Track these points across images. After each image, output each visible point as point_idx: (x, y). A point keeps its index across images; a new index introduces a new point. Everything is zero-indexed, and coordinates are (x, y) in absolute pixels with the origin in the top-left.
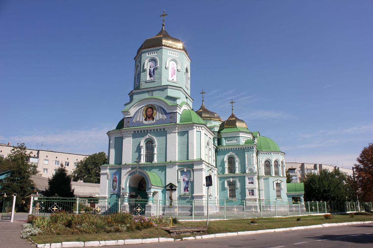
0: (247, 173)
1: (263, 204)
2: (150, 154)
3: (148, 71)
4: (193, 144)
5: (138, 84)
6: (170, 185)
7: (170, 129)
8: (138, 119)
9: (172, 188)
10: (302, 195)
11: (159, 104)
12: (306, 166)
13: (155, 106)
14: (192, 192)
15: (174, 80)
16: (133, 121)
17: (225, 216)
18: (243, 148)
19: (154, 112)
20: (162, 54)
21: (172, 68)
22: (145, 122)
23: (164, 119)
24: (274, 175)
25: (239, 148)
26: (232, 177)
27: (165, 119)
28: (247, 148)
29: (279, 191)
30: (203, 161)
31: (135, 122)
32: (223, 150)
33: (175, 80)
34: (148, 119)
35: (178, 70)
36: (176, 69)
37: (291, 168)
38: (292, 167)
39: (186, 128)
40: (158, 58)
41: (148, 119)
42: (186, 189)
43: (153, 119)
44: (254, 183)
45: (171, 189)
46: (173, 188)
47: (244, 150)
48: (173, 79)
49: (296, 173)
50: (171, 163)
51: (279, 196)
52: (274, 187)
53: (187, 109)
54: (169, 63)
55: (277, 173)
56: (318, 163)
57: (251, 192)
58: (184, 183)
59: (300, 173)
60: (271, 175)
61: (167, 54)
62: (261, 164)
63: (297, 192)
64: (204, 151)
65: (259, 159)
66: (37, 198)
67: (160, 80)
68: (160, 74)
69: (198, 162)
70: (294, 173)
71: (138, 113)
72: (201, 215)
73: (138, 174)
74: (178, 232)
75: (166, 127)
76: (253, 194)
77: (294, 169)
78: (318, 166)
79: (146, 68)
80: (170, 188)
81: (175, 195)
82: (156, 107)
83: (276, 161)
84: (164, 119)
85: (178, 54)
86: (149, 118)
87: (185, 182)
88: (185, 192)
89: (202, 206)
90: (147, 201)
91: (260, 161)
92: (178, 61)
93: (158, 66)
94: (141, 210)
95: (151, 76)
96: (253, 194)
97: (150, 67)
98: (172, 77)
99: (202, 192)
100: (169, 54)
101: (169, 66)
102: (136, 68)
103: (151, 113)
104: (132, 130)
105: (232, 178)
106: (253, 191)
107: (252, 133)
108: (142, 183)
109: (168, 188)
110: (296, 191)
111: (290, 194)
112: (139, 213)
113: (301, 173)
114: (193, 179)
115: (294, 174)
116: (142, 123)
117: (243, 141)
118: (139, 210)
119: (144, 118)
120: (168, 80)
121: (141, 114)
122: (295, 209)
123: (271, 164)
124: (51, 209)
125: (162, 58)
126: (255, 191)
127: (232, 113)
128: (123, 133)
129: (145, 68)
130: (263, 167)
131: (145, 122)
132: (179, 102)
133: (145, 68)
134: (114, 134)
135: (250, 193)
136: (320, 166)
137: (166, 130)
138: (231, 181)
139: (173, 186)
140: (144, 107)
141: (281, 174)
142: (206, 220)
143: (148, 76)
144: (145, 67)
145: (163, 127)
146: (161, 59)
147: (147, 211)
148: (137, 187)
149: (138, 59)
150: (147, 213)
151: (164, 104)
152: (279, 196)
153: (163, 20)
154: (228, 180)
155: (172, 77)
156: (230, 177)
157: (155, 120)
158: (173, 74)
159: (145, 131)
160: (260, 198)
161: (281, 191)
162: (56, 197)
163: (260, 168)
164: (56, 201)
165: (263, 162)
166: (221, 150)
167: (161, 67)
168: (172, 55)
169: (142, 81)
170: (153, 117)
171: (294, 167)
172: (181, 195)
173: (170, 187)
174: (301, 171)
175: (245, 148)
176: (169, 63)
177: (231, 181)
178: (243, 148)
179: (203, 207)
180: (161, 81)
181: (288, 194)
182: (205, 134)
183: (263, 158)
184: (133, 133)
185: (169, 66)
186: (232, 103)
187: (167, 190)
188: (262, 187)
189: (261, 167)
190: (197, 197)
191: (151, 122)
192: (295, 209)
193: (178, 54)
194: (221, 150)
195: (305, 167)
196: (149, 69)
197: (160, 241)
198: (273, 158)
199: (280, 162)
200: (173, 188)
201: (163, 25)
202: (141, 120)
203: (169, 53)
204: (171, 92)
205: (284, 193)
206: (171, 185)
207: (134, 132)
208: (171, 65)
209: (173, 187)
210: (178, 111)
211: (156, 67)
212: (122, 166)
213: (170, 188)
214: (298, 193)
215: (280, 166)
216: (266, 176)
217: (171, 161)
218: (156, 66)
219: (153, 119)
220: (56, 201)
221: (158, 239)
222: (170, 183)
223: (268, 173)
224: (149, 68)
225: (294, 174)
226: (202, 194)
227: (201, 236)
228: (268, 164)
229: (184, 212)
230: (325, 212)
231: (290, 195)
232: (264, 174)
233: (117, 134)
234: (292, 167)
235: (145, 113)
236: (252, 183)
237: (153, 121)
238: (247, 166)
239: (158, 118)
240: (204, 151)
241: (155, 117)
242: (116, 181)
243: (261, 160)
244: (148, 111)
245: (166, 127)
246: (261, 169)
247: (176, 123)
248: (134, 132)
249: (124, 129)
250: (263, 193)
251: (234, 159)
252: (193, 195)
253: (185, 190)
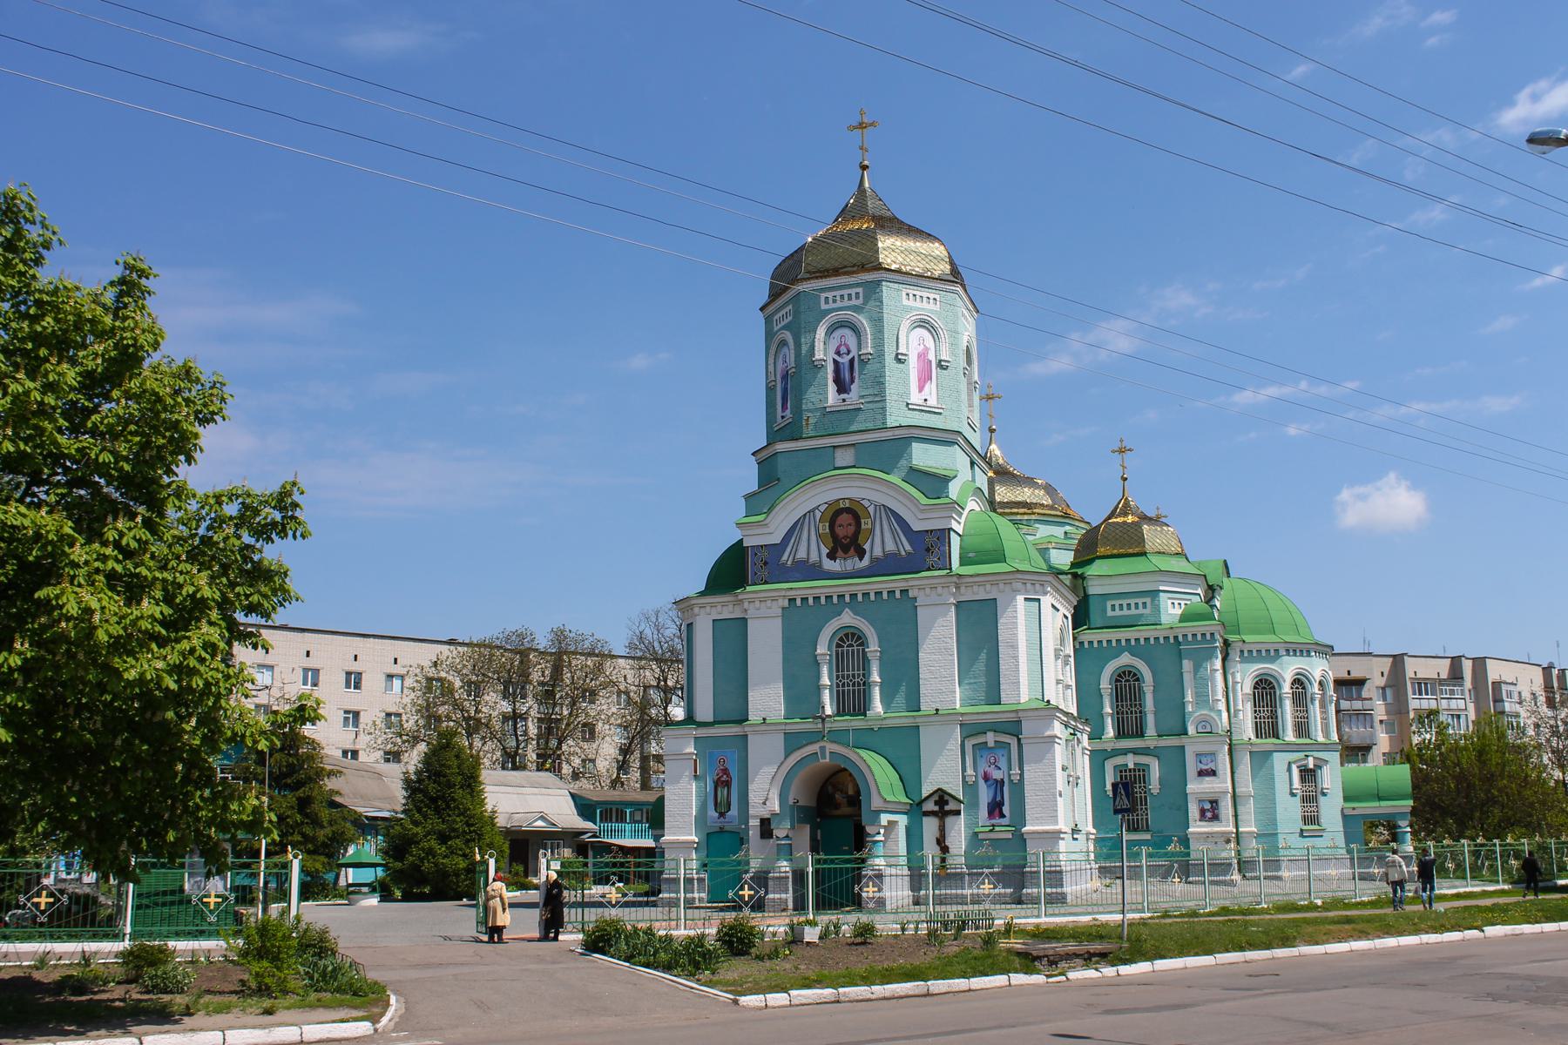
0: (1190, 733)
1: (1252, 849)
2: (854, 685)
3: (830, 368)
4: (1015, 647)
5: (788, 412)
6: (936, 797)
7: (928, 591)
8: (802, 554)
9: (943, 805)
10: (1405, 813)
11: (881, 499)
12: (1412, 668)
13: (866, 503)
14: (1020, 817)
15: (929, 403)
16: (785, 557)
17: (1146, 904)
18: (1176, 638)
19: (863, 526)
20: (882, 302)
21: (919, 356)
22: (829, 565)
23: (903, 553)
24: (1290, 736)
25: (1157, 639)
26: (1135, 752)
27: (909, 554)
28: (1190, 638)
29: (1309, 799)
30: (1057, 708)
31: (789, 563)
32: (1096, 645)
33: (932, 402)
34: (840, 553)
35: (940, 361)
36: (931, 356)
37: (1345, 675)
38: (1349, 673)
39: (988, 587)
40: (865, 318)
41: (840, 553)
42: (995, 808)
43: (861, 554)
44: (1220, 772)
45: (942, 808)
46: (947, 808)
47: (1179, 644)
48: (926, 400)
49: (1371, 699)
50: (937, 718)
51: (1311, 819)
52: (1291, 784)
53: (978, 509)
54: (907, 337)
55: (1302, 729)
56: (1470, 649)
57: (1207, 806)
58: (988, 787)
59: (1385, 699)
60: (1278, 738)
61: (900, 301)
62: (1239, 694)
63: (1383, 803)
64: (1052, 668)
65: (1233, 674)
66: (559, 863)
67: (880, 405)
68: (879, 383)
69: (1036, 713)
70: (1360, 698)
71: (801, 529)
72: (1058, 900)
73: (828, 760)
74: (1051, 958)
75: (911, 583)
76: (1215, 818)
77: (1360, 683)
78: (1467, 667)
79: (822, 356)
80: (936, 808)
81: (959, 833)
82: (871, 510)
83: (1299, 682)
84: (903, 553)
85: (937, 297)
86: (846, 550)
87: (989, 783)
88: (993, 821)
89: (1058, 869)
90: (863, 861)
91: (1235, 683)
92: (939, 324)
93: (870, 350)
94: (752, 892)
95: (842, 387)
96: (1215, 818)
97: (838, 353)
98: (921, 389)
99: (1054, 819)
100: (905, 302)
101: (907, 348)
102: (772, 351)
103: (852, 529)
104: (783, 593)
105: (1135, 754)
106: (1214, 803)
107: (1205, 576)
108: (830, 789)
109: (930, 806)
110: (1380, 798)
111: (1354, 809)
112: (746, 904)
113: (1390, 698)
114: (1022, 775)
115: (1357, 705)
116: (820, 566)
117: (1171, 611)
118: (746, 892)
119: (825, 551)
120: (908, 404)
121: (813, 537)
122: (1371, 870)
123: (1278, 693)
124: (60, 900)
125: (881, 320)
126: (1222, 804)
127: (963, 286)
128: (746, 605)
129: (817, 357)
130: (1249, 706)
131: (829, 565)
132: (954, 489)
133: (817, 357)
134: (708, 608)
135: (1203, 812)
136: (1480, 664)
137: (911, 595)
138: (1131, 766)
139: (946, 797)
140: (822, 508)
141: (1320, 733)
142: (1119, 917)
143: (832, 388)
144: (816, 352)
145: (903, 585)
146: (878, 323)
147: (1439, 889)
148: (814, 804)
149: (783, 312)
150: (941, 895)
151: (901, 498)
152: (1311, 819)
153: (861, 148)
154: (1119, 760)
155: (921, 389)
156: (1116, 753)
157: (867, 557)
158: (925, 378)
159: (832, 596)
160: (1240, 829)
161: (1322, 799)
162: (614, 857)
163: (1237, 711)
164: (614, 870)
165: (1248, 688)
166: (1086, 645)
167: (880, 354)
168: (839, 304)
169: (810, 406)
170: (859, 545)
171: (1355, 674)
172: (977, 830)
173: (936, 803)
174: (1389, 692)
175: (1180, 639)
176: (907, 337)
177: (1131, 766)
178: (1176, 638)
179: (1061, 872)
180: (884, 408)
181: (1347, 812)
182: (1053, 606)
183: (1245, 677)
184: (786, 603)
185: (907, 348)
186: (1121, 451)
187: (927, 814)
188: (1247, 786)
189: (1240, 707)
190: (1038, 836)
191: (854, 564)
192: (1371, 870)
193: (937, 297)
194: (1086, 645)
195: (1410, 674)
196: (835, 361)
197: (1013, 982)
198: (1287, 670)
199: (1316, 685)
200: (947, 808)
201: (864, 168)
202: (814, 557)
203: (904, 294)
204: (924, 456)
205: (1331, 809)
206: (941, 797)
207: (790, 600)
208: (914, 343)
209: (947, 803)
210: (954, 525)
211: (860, 355)
212: (751, 729)
213: (936, 808)
214: (1385, 807)
215: (1313, 700)
216: (1259, 741)
217: (937, 710)
218: (860, 348)
219: (861, 554)
220: (614, 870)
221: (1006, 977)
222: (939, 789)
223: (1268, 727)
224: (832, 355)
225: (1357, 705)
226: (1057, 827)
227: (1115, 968)
228: (1265, 689)
229: (954, 891)
230: (1498, 882)
231: (1355, 812)
232: (1249, 733)
233: (719, 607)
234: (1349, 673)
235: (828, 530)
236: (1213, 773)
237: (861, 560)
238: (1189, 708)
239: (878, 552)
240: (1052, 668)
241: (867, 547)
242: (728, 784)
243: (1238, 679)
244: (838, 523)
245: (911, 583)
246: (1241, 715)
247: (951, 569)
248: (790, 600)
249: (749, 588)
250: (1249, 811)
251: (1138, 680)
252: (1024, 830)
253: (991, 814)
